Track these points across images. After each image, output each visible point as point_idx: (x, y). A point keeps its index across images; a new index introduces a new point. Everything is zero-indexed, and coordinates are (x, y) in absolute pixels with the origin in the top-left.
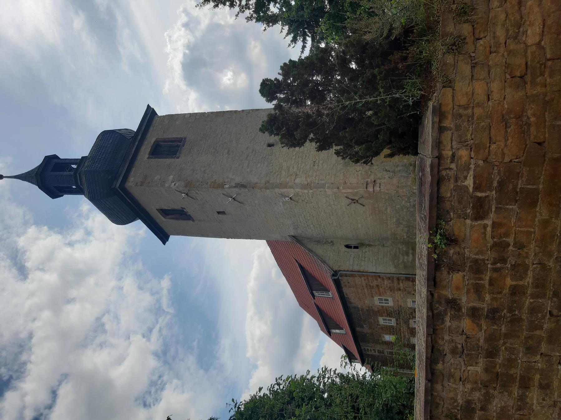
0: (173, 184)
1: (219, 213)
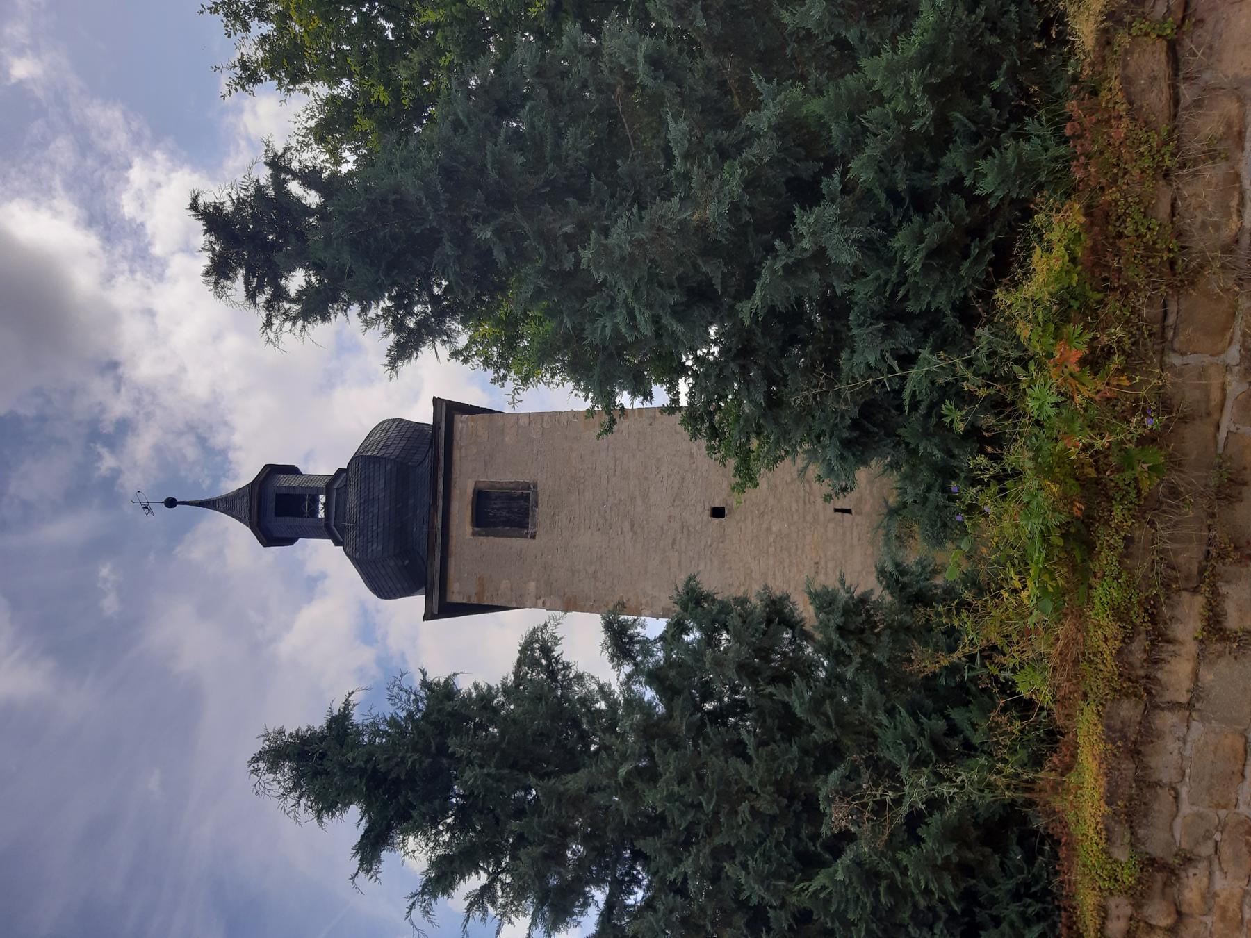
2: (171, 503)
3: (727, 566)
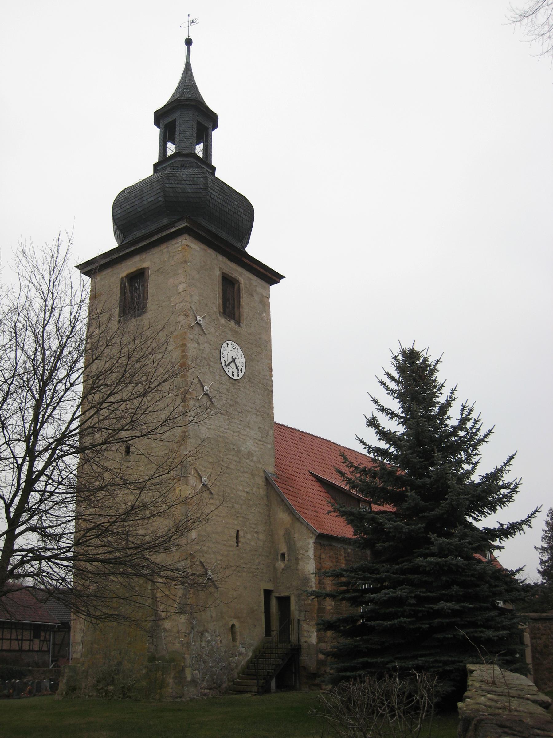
2: (189, 42)
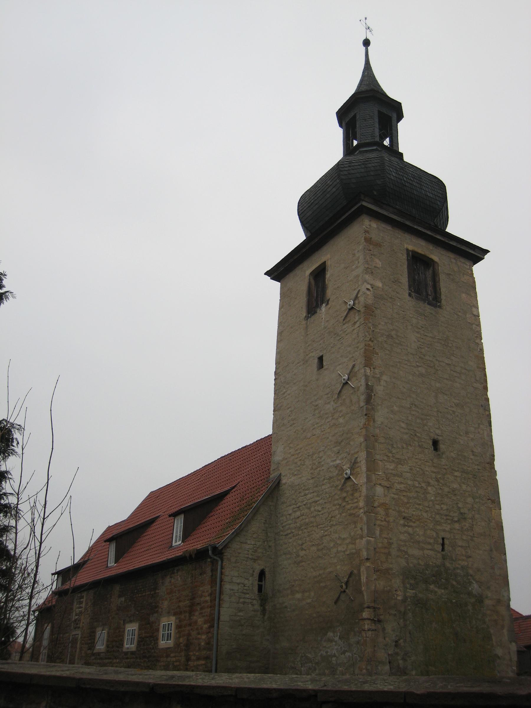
0: (369, 287)
1: (321, 359)
2: (367, 43)
3: (405, 446)
